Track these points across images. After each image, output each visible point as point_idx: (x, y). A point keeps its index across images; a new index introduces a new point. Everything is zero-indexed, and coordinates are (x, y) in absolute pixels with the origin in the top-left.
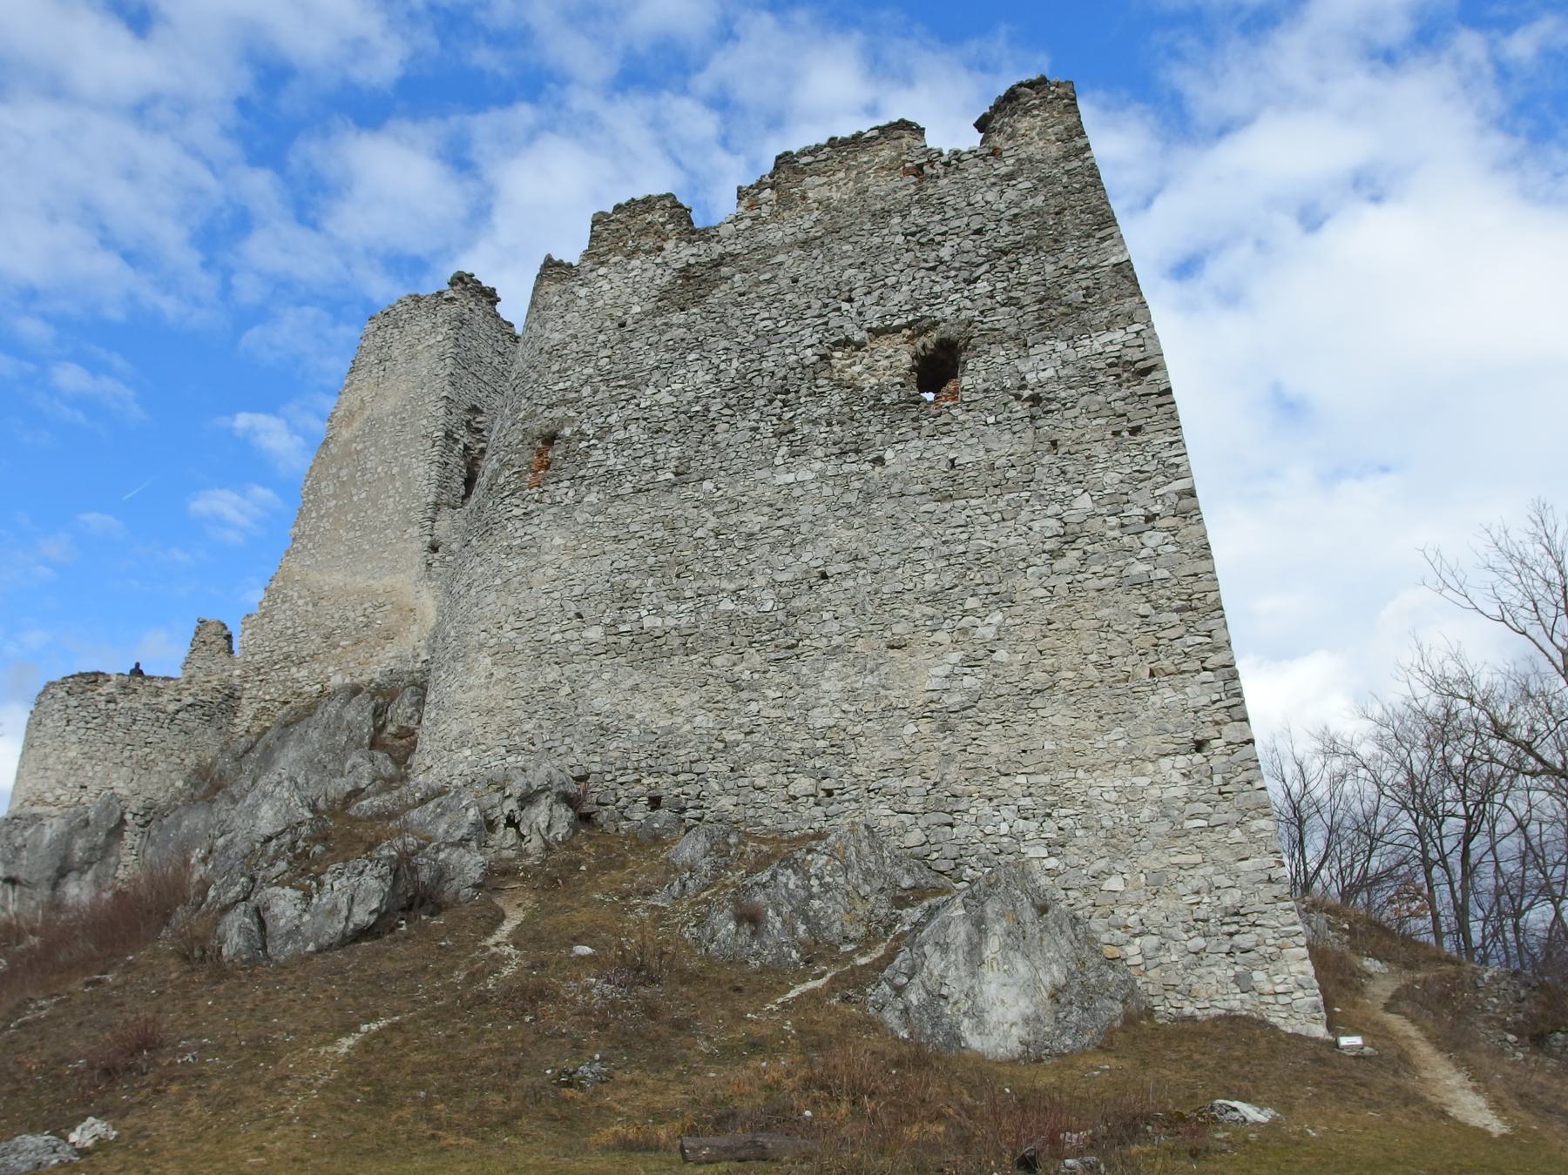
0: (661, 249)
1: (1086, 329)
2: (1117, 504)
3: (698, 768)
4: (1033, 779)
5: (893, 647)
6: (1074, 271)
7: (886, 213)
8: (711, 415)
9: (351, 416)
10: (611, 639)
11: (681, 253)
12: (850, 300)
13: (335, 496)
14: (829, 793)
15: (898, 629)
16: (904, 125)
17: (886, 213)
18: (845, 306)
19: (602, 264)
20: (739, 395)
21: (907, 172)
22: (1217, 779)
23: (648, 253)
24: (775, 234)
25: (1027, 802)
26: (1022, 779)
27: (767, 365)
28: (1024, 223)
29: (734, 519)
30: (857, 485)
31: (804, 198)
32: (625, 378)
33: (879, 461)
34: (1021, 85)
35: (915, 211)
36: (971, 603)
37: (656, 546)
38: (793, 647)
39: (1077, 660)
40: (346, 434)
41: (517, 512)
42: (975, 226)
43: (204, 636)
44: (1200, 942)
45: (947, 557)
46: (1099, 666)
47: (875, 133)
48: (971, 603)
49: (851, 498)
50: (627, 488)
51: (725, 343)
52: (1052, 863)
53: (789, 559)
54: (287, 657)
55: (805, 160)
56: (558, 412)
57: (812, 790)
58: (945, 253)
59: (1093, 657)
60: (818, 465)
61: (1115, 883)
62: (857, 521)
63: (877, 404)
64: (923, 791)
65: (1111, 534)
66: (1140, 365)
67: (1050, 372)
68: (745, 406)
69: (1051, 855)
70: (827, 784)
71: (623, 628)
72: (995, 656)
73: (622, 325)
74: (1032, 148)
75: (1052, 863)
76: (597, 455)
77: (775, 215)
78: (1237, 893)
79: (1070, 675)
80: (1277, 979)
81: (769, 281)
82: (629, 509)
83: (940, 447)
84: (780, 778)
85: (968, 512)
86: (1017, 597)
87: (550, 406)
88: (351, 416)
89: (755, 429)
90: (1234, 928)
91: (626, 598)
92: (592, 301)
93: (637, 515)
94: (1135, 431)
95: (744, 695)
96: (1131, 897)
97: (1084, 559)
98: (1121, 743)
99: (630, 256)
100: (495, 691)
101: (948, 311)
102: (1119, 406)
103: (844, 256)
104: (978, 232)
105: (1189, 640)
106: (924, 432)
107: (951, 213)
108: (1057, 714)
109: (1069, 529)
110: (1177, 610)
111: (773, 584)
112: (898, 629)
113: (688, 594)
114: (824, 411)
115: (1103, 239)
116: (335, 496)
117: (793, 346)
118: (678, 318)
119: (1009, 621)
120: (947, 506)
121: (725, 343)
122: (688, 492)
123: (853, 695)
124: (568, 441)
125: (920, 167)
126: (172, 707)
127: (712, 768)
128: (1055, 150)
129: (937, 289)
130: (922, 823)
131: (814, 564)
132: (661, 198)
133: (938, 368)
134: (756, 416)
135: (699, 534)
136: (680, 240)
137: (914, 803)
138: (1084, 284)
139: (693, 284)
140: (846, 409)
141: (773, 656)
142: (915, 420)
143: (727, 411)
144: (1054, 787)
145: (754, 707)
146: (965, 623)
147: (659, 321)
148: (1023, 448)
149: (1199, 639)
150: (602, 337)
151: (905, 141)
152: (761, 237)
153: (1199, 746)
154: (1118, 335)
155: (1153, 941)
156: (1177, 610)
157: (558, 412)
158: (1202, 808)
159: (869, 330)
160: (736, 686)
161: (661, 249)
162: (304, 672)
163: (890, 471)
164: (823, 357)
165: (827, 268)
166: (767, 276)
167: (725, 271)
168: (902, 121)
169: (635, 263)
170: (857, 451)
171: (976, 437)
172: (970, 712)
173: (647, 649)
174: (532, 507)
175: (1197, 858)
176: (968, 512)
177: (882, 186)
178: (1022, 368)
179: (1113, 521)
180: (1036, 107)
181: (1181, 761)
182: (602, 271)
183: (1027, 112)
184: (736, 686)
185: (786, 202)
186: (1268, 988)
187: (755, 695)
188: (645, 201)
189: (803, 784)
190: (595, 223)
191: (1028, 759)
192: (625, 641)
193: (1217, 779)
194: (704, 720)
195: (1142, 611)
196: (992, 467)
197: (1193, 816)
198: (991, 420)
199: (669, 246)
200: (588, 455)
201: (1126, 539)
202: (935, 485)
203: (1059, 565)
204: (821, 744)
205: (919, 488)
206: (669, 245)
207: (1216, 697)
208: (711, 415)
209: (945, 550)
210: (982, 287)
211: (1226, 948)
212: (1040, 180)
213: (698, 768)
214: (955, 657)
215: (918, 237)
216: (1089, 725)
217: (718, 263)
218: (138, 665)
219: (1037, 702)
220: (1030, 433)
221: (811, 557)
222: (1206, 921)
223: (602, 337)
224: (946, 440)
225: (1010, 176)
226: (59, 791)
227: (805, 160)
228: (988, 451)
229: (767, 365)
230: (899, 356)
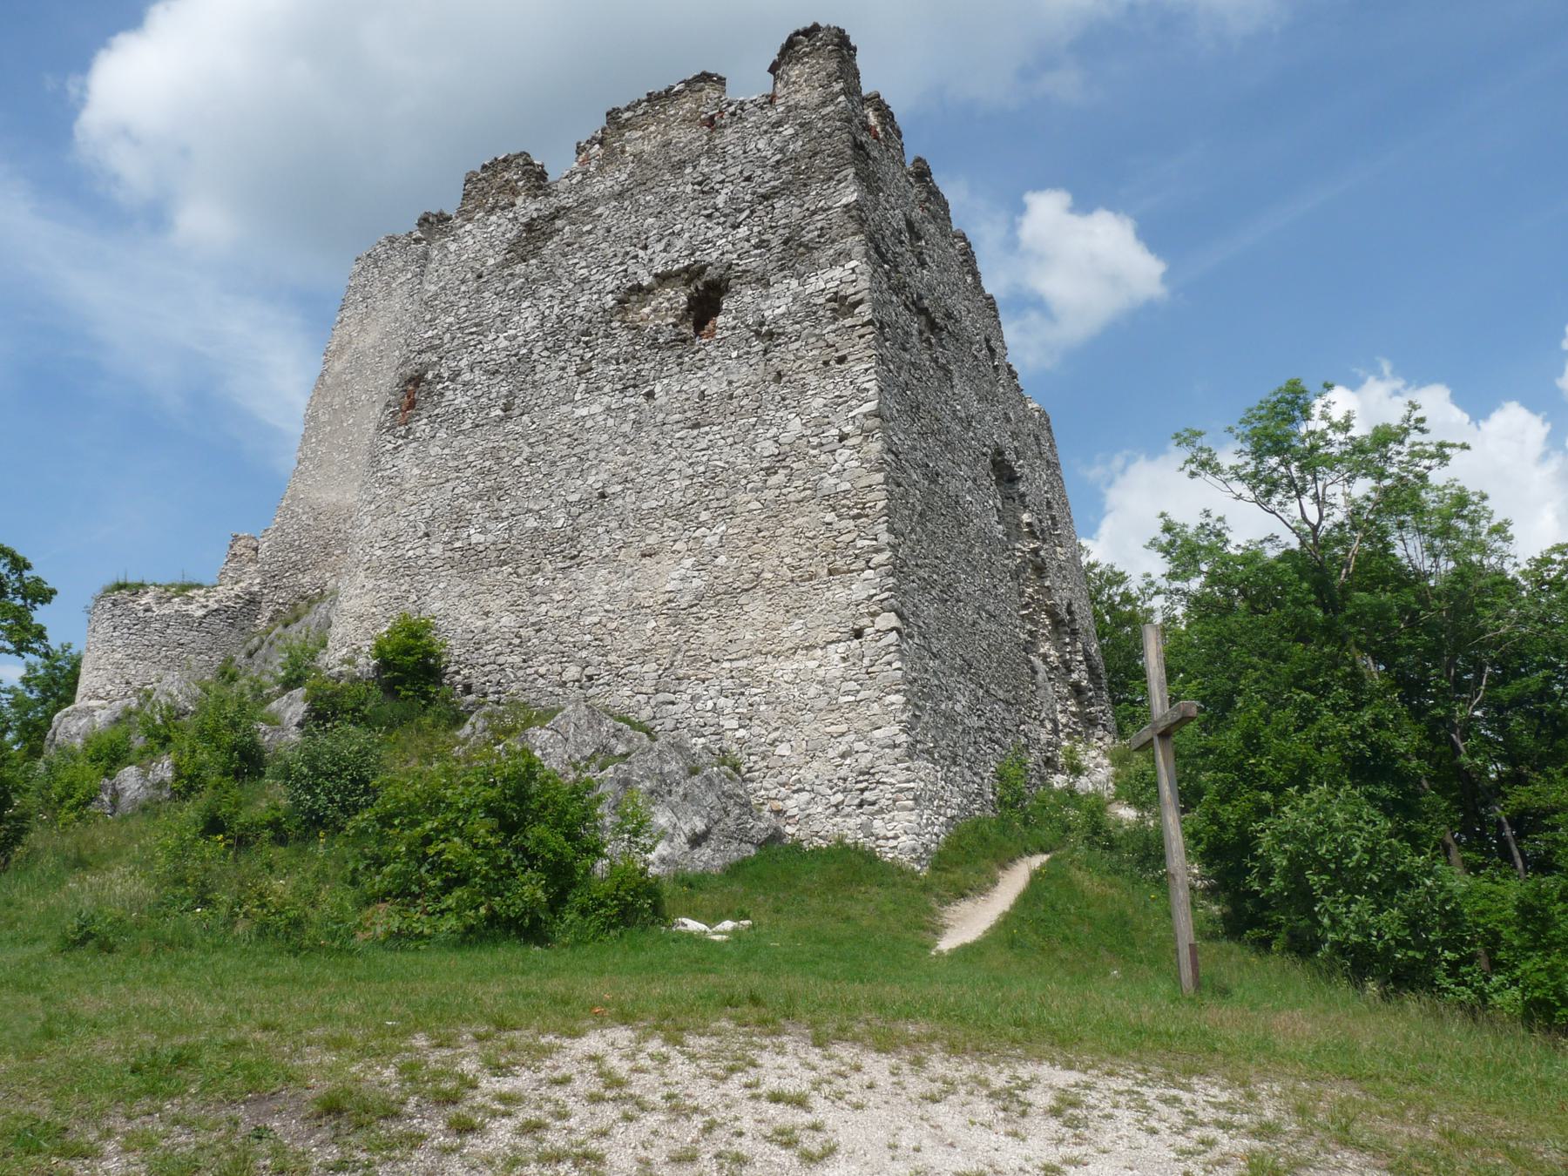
0: (513, 205)
1: (816, 267)
2: (822, 423)
3: (501, 660)
4: (735, 664)
5: (644, 556)
6: (814, 213)
7: (682, 164)
8: (534, 357)
9: (341, 348)
10: (449, 554)
11: (528, 208)
12: (645, 248)
13: (330, 423)
14: (590, 678)
15: (650, 540)
16: (705, 77)
17: (682, 164)
18: (641, 253)
19: (469, 220)
20: (556, 336)
21: (703, 123)
22: (866, 661)
23: (503, 209)
24: (600, 186)
25: (727, 683)
26: (727, 665)
27: (579, 311)
28: (784, 169)
29: (542, 448)
30: (633, 416)
31: (623, 152)
32: (476, 325)
33: (650, 395)
34: (797, 33)
35: (703, 161)
36: (704, 516)
37: (485, 473)
38: (573, 558)
39: (776, 562)
40: (338, 366)
41: (389, 446)
42: (746, 174)
43: (238, 549)
44: (840, 797)
45: (691, 477)
46: (792, 568)
47: (681, 87)
48: (704, 516)
49: (626, 428)
50: (468, 425)
51: (550, 291)
52: (741, 733)
53: (579, 482)
54: (295, 564)
55: (627, 115)
56: (425, 357)
57: (577, 676)
58: (720, 200)
59: (788, 560)
60: (606, 399)
61: (783, 749)
62: (629, 449)
63: (654, 345)
64: (655, 675)
65: (813, 452)
66: (851, 299)
67: (783, 309)
68: (556, 349)
69: (741, 727)
70: (590, 671)
71: (458, 544)
72: (718, 561)
73: (480, 276)
74: (799, 96)
75: (741, 733)
76: (449, 395)
77: (600, 168)
78: (869, 756)
79: (770, 576)
80: (890, 827)
81: (589, 232)
82: (469, 441)
83: (694, 383)
84: (557, 668)
85: (711, 437)
86: (738, 510)
87: (420, 352)
88: (341, 348)
89: (563, 369)
90: (865, 784)
91: (460, 520)
92: (460, 256)
93: (474, 446)
94: (841, 360)
95: (537, 599)
96: (794, 761)
97: (790, 478)
98: (800, 633)
99: (491, 211)
100: (367, 600)
101: (715, 255)
102: (831, 338)
103: (647, 205)
104: (748, 179)
105: (859, 543)
106: (685, 367)
107: (730, 161)
108: (756, 608)
109: (782, 449)
110: (855, 518)
111: (567, 503)
112: (650, 540)
113: (504, 515)
114: (615, 351)
115: (840, 182)
116: (330, 423)
117: (599, 292)
118: (520, 268)
119: (730, 531)
120: (695, 432)
121: (550, 291)
122: (510, 426)
123: (612, 596)
124: (430, 383)
125: (712, 117)
126: (201, 613)
127: (510, 660)
128: (816, 96)
129: (710, 234)
130: (653, 702)
131: (596, 486)
132: (516, 157)
133: (705, 304)
134: (565, 357)
135: (516, 463)
136: (528, 195)
137: (648, 687)
138: (819, 225)
139: (535, 233)
140: (630, 349)
141: (560, 565)
142: (680, 356)
143: (545, 353)
144: (749, 671)
145: (544, 608)
146: (698, 533)
147: (506, 272)
148: (755, 378)
149: (867, 542)
150: (463, 288)
151: (704, 93)
152: (588, 190)
153: (858, 634)
154: (837, 272)
155: (805, 796)
156: (855, 518)
157: (425, 357)
158: (853, 685)
159: (656, 275)
160: (532, 592)
161: (513, 205)
162: (308, 578)
163: (657, 403)
164: (620, 302)
165: (633, 219)
166: (589, 227)
167: (559, 223)
168: (704, 74)
169: (493, 218)
170: (635, 386)
171: (722, 368)
172: (695, 609)
173: (469, 561)
174: (400, 442)
175: (843, 728)
176: (711, 437)
177: (684, 136)
178: (763, 306)
179: (815, 441)
180: (806, 54)
181: (842, 647)
182: (469, 227)
183: (799, 60)
184: (532, 592)
185: (611, 156)
186: (882, 833)
187: (544, 599)
188: (505, 160)
189: (572, 672)
190: (468, 181)
191: (733, 648)
192: (457, 555)
193: (866, 661)
194: (508, 620)
195: (827, 519)
196: (731, 397)
197: (847, 693)
198: (734, 354)
199: (519, 201)
200: (442, 395)
201: (823, 457)
202: (689, 414)
203: (773, 480)
204: (588, 637)
205: (677, 417)
206: (519, 201)
207: (873, 592)
208: (534, 357)
209: (690, 472)
210: (743, 231)
211: (857, 801)
212: (802, 125)
213: (501, 660)
214: (688, 562)
215: (705, 187)
216: (779, 618)
217: (554, 217)
218: (53, 592)
219: (743, 599)
220: (762, 365)
221: (594, 480)
222: (845, 780)
223: (463, 288)
224: (700, 374)
225: (779, 124)
226: (109, 687)
227: (627, 115)
228: (730, 383)
229: (579, 311)
230: (679, 297)
